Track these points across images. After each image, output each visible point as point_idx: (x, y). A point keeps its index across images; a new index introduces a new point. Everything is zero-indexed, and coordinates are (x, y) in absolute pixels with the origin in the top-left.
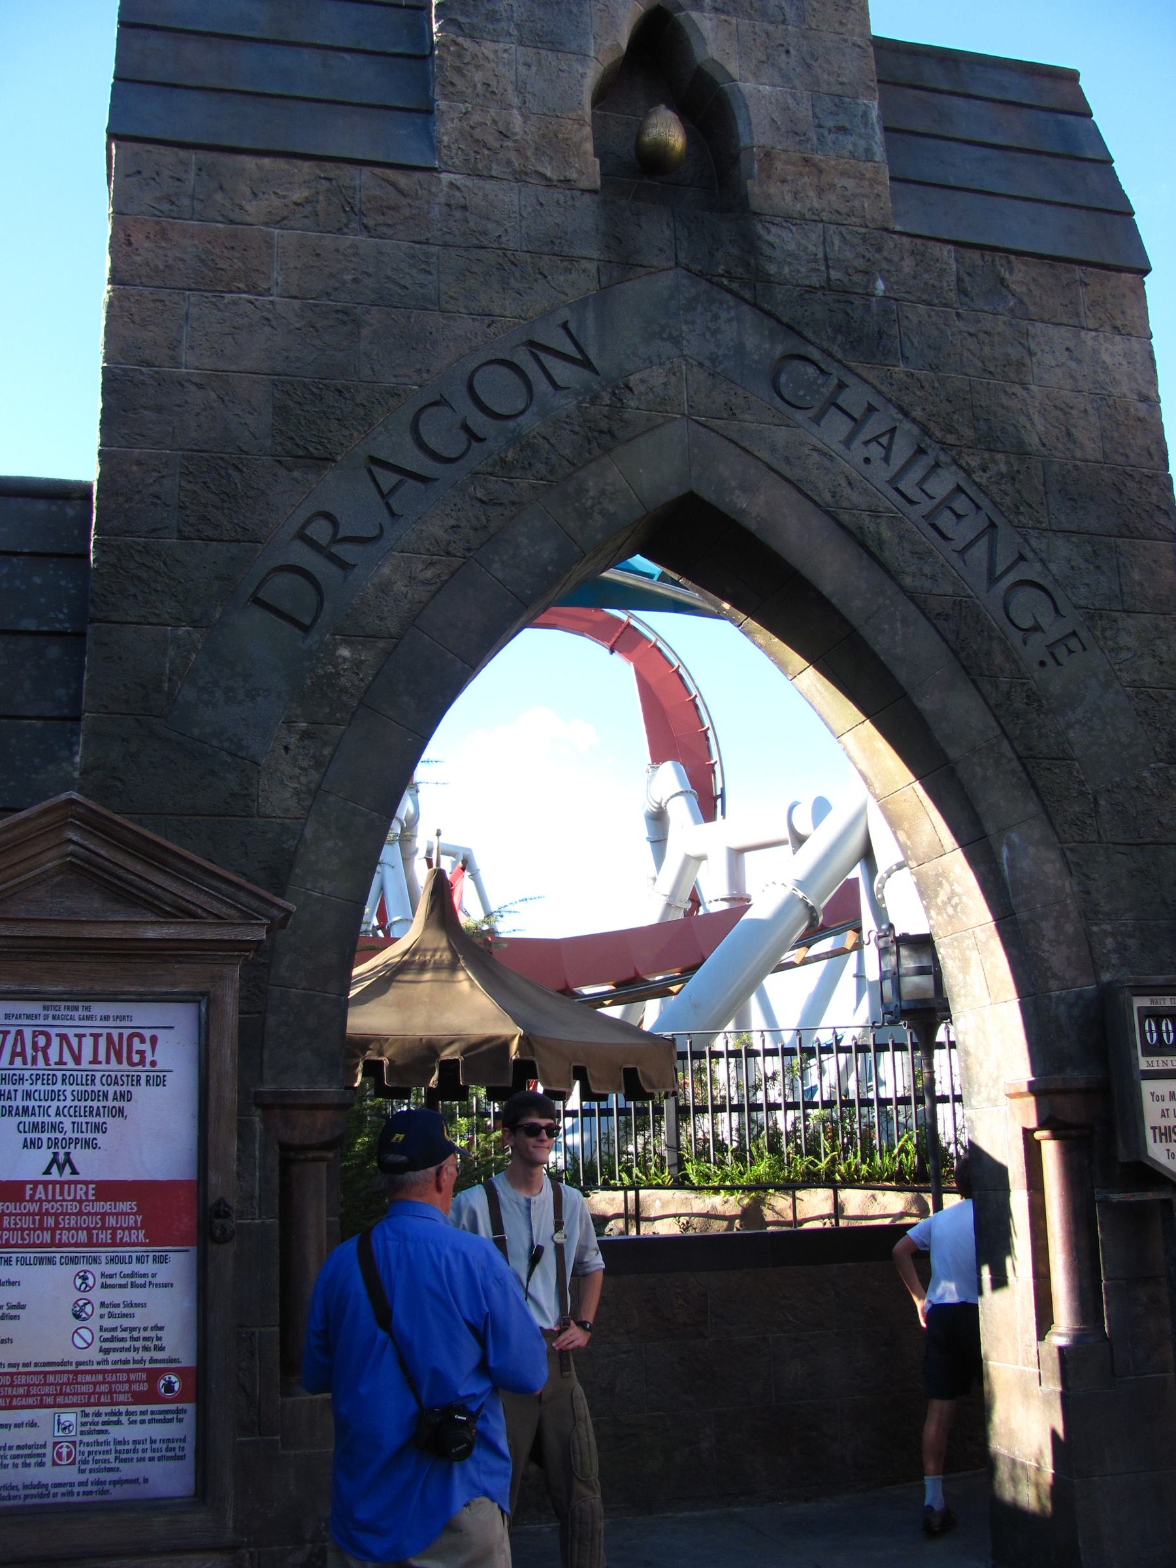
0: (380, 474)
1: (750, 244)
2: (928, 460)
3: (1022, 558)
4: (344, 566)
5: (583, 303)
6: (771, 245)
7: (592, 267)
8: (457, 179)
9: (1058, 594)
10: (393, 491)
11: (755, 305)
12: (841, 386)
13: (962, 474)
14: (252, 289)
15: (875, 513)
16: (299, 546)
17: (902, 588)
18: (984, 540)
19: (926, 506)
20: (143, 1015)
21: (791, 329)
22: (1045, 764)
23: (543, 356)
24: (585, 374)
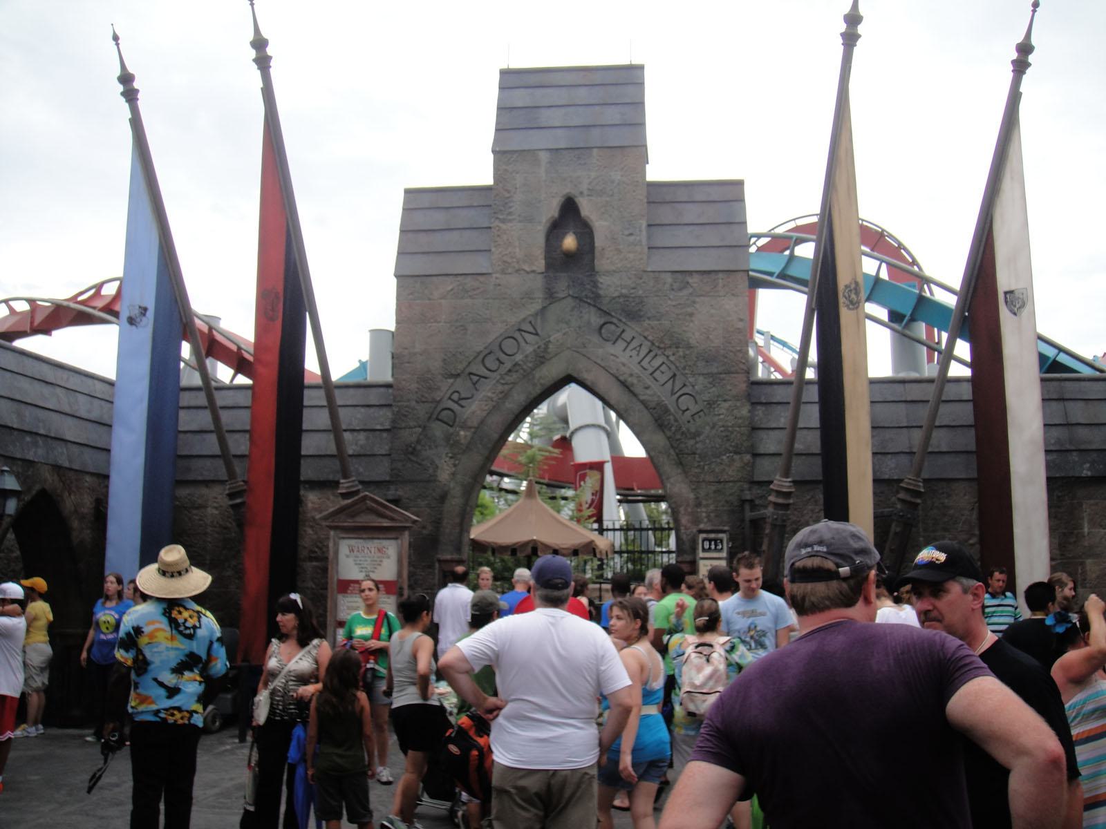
0: (472, 377)
1: (595, 284)
2: (652, 354)
3: (685, 385)
4: (462, 407)
5: (537, 314)
6: (601, 283)
7: (540, 301)
8: (498, 275)
9: (697, 397)
10: (477, 382)
11: (595, 306)
12: (623, 331)
13: (665, 358)
14: (436, 321)
15: (631, 375)
16: (450, 402)
17: (639, 399)
18: (671, 381)
19: (651, 370)
20: (385, 543)
21: (607, 313)
22: (686, 456)
23: (523, 333)
24: (536, 337)
